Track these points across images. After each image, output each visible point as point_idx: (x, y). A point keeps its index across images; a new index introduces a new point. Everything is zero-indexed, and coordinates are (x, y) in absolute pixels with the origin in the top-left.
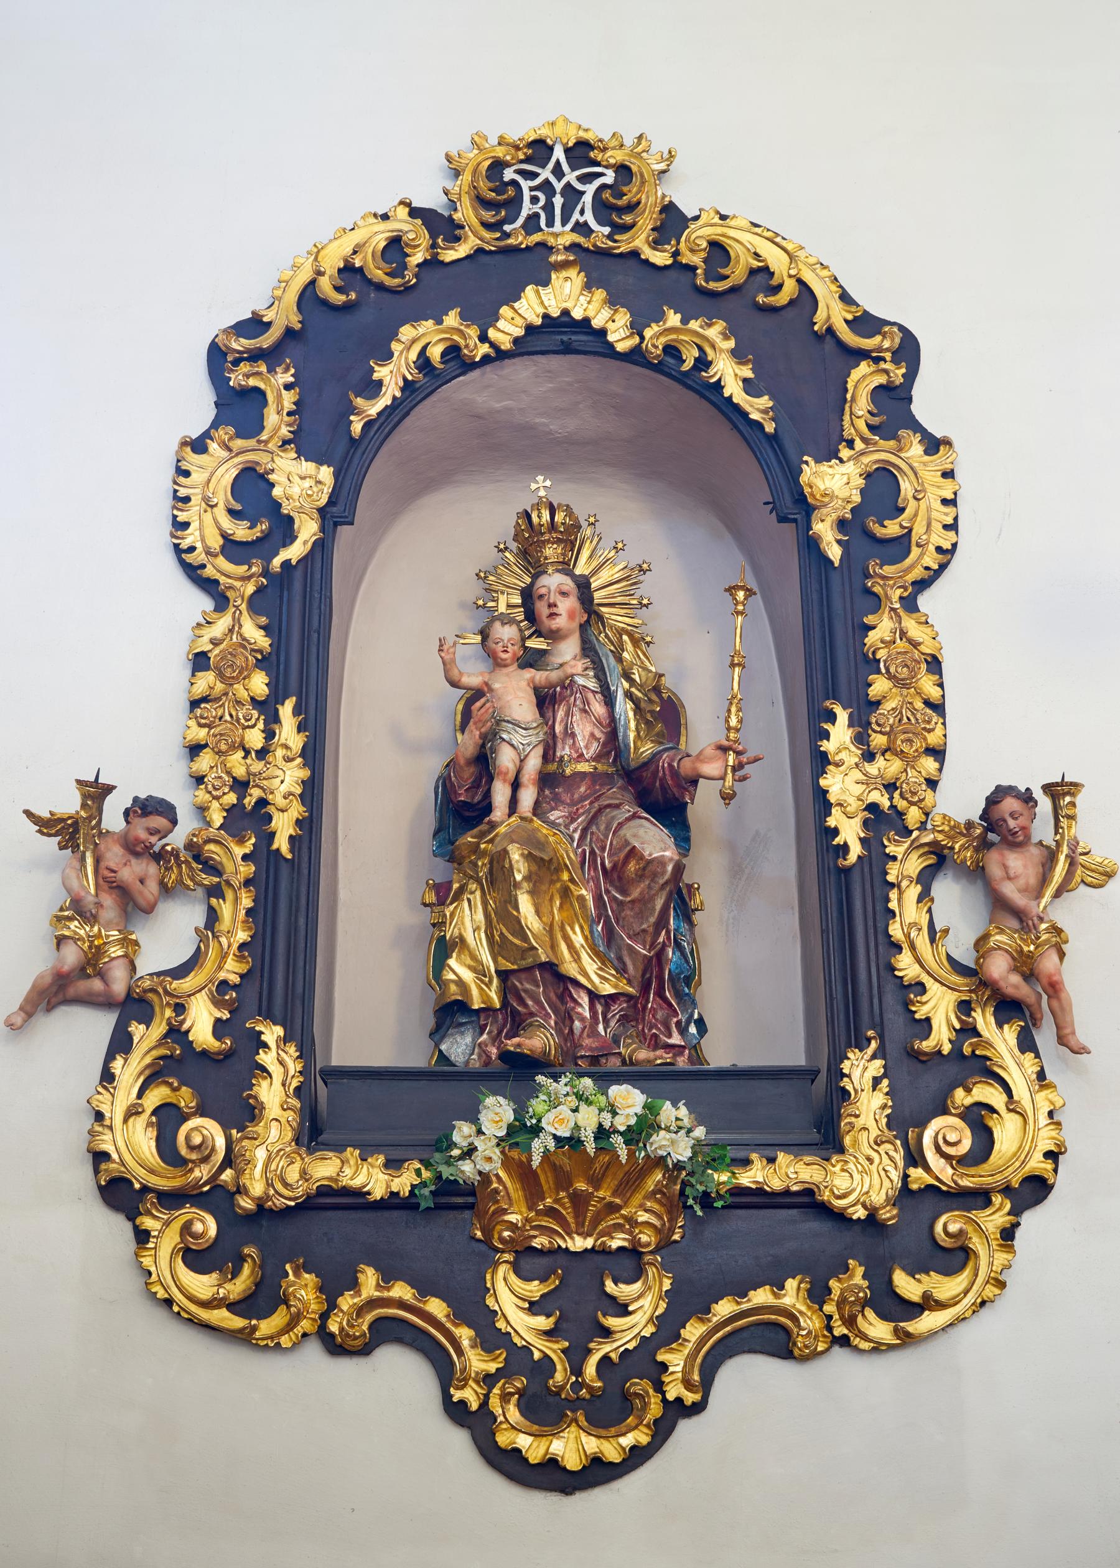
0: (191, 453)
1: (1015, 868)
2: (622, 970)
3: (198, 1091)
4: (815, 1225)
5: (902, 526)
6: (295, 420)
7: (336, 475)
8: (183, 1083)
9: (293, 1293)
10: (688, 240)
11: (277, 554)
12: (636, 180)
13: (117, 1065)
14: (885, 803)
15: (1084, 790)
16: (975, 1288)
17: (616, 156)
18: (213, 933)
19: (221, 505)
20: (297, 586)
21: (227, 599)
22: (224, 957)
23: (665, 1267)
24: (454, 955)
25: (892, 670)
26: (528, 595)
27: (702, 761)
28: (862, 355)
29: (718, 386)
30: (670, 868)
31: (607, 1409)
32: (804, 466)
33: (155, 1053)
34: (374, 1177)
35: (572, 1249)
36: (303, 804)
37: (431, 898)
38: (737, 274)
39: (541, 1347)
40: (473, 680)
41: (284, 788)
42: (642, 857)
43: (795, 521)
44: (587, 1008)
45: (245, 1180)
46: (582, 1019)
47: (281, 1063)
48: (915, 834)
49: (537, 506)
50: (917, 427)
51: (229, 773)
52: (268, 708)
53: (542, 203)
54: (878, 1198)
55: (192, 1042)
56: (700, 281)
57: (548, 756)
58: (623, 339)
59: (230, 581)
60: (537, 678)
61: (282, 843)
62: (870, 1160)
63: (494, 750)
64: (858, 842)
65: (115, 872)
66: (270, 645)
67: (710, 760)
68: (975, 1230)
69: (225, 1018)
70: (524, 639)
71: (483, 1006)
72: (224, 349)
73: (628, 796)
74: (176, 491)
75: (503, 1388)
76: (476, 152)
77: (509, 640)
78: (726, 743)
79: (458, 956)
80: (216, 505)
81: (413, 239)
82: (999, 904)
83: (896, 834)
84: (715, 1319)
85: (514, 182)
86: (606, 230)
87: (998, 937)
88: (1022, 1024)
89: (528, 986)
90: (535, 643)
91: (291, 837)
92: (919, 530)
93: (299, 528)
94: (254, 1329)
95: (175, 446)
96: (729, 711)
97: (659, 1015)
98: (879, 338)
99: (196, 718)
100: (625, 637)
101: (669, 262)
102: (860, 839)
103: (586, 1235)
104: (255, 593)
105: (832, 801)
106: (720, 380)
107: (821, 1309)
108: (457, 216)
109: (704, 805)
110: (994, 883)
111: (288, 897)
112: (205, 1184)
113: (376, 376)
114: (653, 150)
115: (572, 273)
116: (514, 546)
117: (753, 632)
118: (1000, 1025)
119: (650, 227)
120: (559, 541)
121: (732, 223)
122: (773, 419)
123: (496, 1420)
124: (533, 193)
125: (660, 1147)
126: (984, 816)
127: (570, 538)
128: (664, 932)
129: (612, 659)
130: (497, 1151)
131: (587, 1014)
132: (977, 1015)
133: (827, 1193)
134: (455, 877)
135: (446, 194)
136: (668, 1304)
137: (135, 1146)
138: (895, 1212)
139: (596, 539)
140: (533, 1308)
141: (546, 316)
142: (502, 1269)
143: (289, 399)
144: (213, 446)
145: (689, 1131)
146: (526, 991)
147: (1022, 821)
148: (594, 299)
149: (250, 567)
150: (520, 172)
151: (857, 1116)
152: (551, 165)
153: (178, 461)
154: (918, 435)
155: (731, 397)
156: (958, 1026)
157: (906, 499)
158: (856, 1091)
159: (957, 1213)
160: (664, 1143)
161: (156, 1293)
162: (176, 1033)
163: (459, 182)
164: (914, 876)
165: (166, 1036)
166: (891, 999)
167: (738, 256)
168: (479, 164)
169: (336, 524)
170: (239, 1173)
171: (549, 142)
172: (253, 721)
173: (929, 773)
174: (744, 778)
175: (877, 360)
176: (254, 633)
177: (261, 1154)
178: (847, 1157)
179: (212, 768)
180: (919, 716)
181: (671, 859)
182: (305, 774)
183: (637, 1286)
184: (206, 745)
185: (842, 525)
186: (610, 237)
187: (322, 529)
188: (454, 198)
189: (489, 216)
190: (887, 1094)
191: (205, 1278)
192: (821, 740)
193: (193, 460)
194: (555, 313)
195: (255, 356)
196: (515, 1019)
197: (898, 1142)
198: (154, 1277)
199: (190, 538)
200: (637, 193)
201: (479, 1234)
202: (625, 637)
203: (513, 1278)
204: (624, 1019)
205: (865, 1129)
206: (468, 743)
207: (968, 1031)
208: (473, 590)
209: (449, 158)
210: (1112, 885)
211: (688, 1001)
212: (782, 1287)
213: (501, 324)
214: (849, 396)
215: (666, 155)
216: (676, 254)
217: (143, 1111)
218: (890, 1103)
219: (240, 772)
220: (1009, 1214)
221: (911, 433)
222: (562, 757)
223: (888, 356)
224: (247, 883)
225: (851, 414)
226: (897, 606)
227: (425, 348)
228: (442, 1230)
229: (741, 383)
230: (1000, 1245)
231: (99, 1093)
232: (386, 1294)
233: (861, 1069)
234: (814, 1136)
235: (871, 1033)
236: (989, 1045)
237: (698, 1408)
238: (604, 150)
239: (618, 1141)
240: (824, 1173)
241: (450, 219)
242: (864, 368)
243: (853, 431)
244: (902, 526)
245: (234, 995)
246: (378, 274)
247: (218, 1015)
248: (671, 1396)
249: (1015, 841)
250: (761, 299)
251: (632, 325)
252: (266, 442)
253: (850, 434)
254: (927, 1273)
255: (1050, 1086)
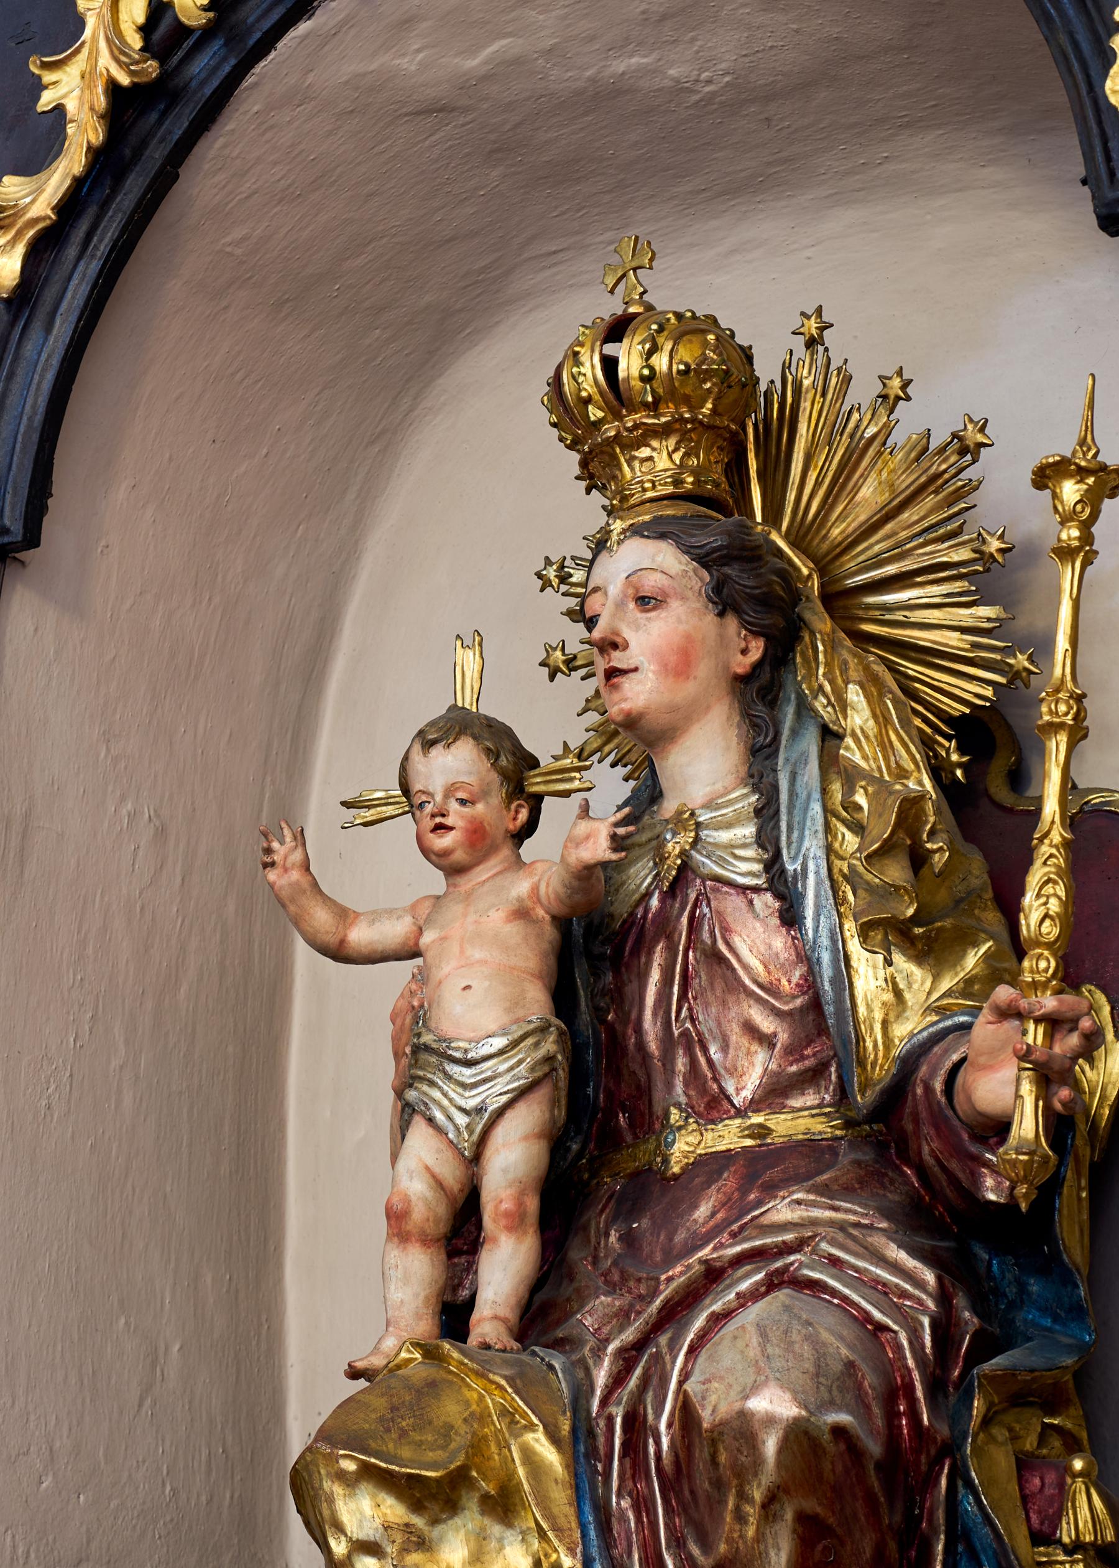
77: (449, 792)
110: (573, 1482)
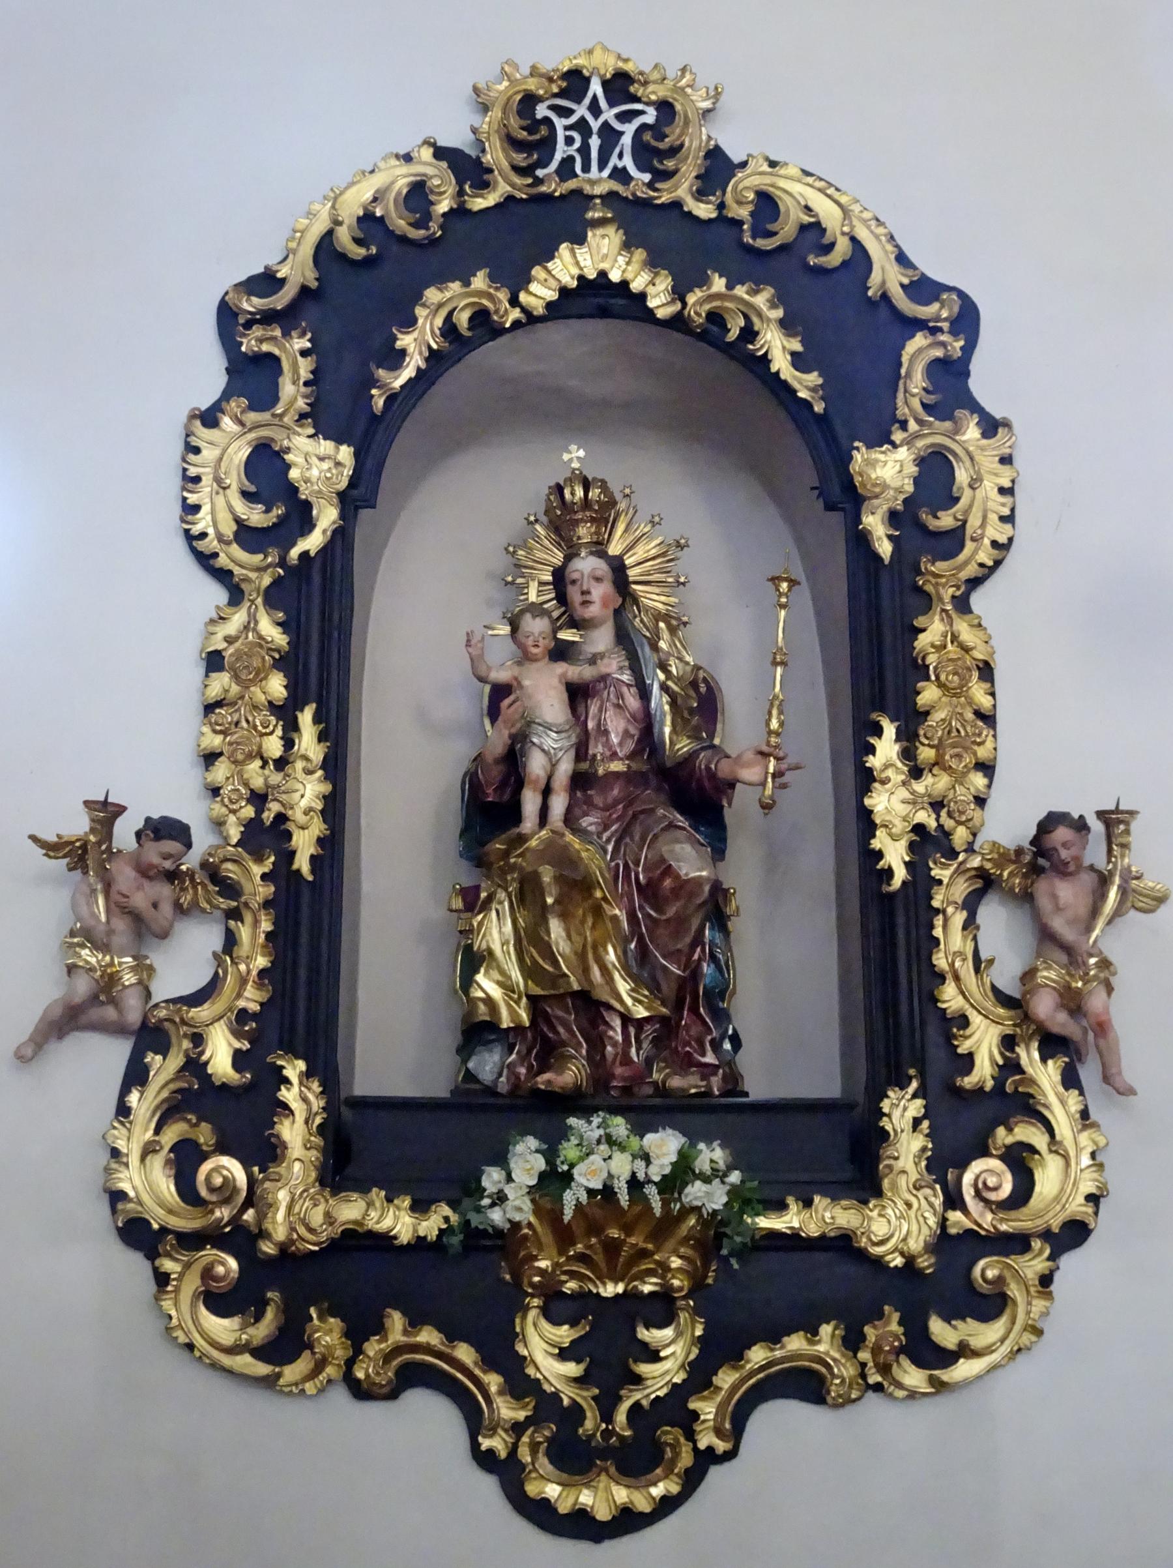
0: (201, 427)
1: (1068, 894)
2: (655, 988)
3: (218, 1130)
4: (851, 1269)
5: (957, 519)
6: (312, 391)
7: (357, 455)
8: (200, 1119)
9: (318, 1338)
10: (735, 188)
11: (294, 544)
12: (679, 120)
13: (133, 1098)
14: (932, 824)
15: (1139, 816)
16: (1012, 1336)
17: (656, 92)
18: (231, 957)
19: (235, 487)
20: (317, 579)
21: (242, 592)
22: (243, 981)
23: (697, 1312)
24: (482, 970)
25: (943, 677)
26: (560, 579)
27: (743, 766)
28: (919, 325)
29: (765, 360)
30: (707, 888)
31: (637, 1460)
32: (855, 453)
33: (172, 1087)
34: (401, 1220)
35: (604, 1294)
36: (324, 821)
37: (458, 903)
38: (786, 231)
39: (568, 1394)
40: (501, 675)
41: (304, 803)
42: (678, 877)
43: (843, 509)
44: (619, 1030)
45: (268, 1225)
46: (615, 1045)
47: (305, 1100)
48: (961, 857)
49: (570, 481)
50: (975, 407)
51: (246, 784)
52: (286, 713)
53: (577, 145)
54: (915, 1245)
55: (211, 1075)
56: (747, 239)
57: (581, 751)
58: (663, 305)
59: (244, 572)
60: (570, 674)
61: (302, 863)
62: (909, 1205)
63: (523, 753)
64: (903, 866)
65: (128, 897)
66: (288, 643)
67: (748, 765)
68: (1013, 1277)
69: (244, 1048)
70: (555, 632)
71: (512, 1025)
72: (234, 309)
73: (663, 797)
74: (185, 470)
75: (532, 1437)
76: (506, 83)
78: (765, 749)
79: (486, 972)
80: (228, 487)
81: (439, 186)
82: (1046, 936)
83: (943, 857)
84: (748, 1366)
85: (547, 121)
86: (647, 177)
87: (1045, 974)
88: (1066, 1059)
89: (560, 1013)
90: (566, 635)
91: (312, 856)
92: (974, 522)
93: (319, 514)
94: (279, 1376)
95: (183, 417)
96: (770, 713)
97: (693, 1032)
98: (936, 306)
99: (211, 724)
100: (662, 625)
101: (714, 215)
102: (906, 863)
103: (616, 1281)
104: (272, 584)
105: (878, 821)
106: (766, 353)
107: (855, 1356)
108: (488, 159)
109: (740, 810)
111: (309, 919)
112: (226, 1225)
113: (399, 344)
114: (699, 82)
115: (610, 230)
116: (544, 519)
117: (793, 623)
118: (1044, 1060)
119: (694, 174)
120: (592, 520)
121: (782, 172)
122: (822, 398)
123: (524, 1470)
124: (568, 133)
125: (696, 1198)
126: (1035, 841)
127: (604, 514)
128: (699, 949)
129: (647, 649)
130: (527, 1200)
131: (620, 1038)
132: (1021, 1051)
133: (864, 1240)
134: (483, 885)
135: (474, 133)
136: (700, 1350)
137: (151, 1186)
138: (933, 1260)
139: (631, 511)
140: (564, 1354)
141: (581, 278)
142: (532, 1314)
143: (305, 367)
144: (227, 422)
145: (725, 1175)
146: (558, 1018)
147: (1073, 851)
148: (634, 259)
149: (266, 557)
150: (552, 108)
151: (896, 1158)
152: (587, 101)
153: (187, 435)
154: (975, 416)
155: (778, 373)
156: (1001, 1062)
157: (961, 488)
158: (895, 1130)
159: (995, 1258)
160: (699, 1194)
161: (176, 1338)
162: (195, 1066)
163: (487, 119)
164: (960, 902)
165: (182, 1069)
166: (933, 1033)
167: (788, 210)
168: (509, 99)
169: (357, 508)
170: (261, 1217)
171: (586, 73)
172: (271, 728)
173: (978, 790)
174: (784, 786)
175: (934, 331)
176: (270, 630)
177: (283, 1196)
178: (886, 1202)
179: (228, 778)
180: (969, 729)
181: (707, 879)
182: (326, 788)
183: (668, 1332)
184: (221, 754)
185: (894, 518)
186: (650, 185)
187: (343, 516)
188: (483, 137)
189: (520, 159)
190: (927, 1136)
191: (225, 1322)
192: (867, 755)
193: (203, 434)
194: (591, 275)
195: (268, 318)
196: (548, 1053)
197: (938, 1187)
198: (175, 1322)
199: (202, 522)
200: (680, 136)
201: (508, 1277)
202: (662, 625)
203: (545, 1325)
204: (656, 1042)
205: (904, 1172)
206: (497, 739)
207: (1011, 1067)
208: (500, 562)
209: (476, 90)
210: (1163, 910)
211: (721, 1017)
212: (815, 1333)
213: (534, 287)
214: (903, 371)
215: (712, 93)
216: (721, 206)
217: (162, 1148)
218: (930, 1146)
219: (258, 783)
220: (1048, 1259)
221: (967, 413)
222: (595, 755)
223: (945, 325)
224: (267, 904)
225: (906, 391)
226: (949, 607)
227: (451, 314)
228: (472, 1286)
229: (789, 357)
230: (1039, 1292)
231: (115, 1128)
232: (412, 1340)
233: (902, 1110)
234: (848, 1173)
235: (912, 1072)
236: (1032, 1082)
237: (730, 1455)
238: (645, 83)
239: (651, 1191)
240: (860, 1217)
241: (478, 162)
242: (919, 340)
243: (906, 410)
244: (957, 519)
245: (254, 1025)
246: (400, 224)
247: (237, 1045)
248: (702, 1445)
249: (1063, 870)
250: (812, 260)
251: (675, 290)
252: (281, 416)
253: (904, 414)
254: (963, 1319)
255: (1095, 1125)
